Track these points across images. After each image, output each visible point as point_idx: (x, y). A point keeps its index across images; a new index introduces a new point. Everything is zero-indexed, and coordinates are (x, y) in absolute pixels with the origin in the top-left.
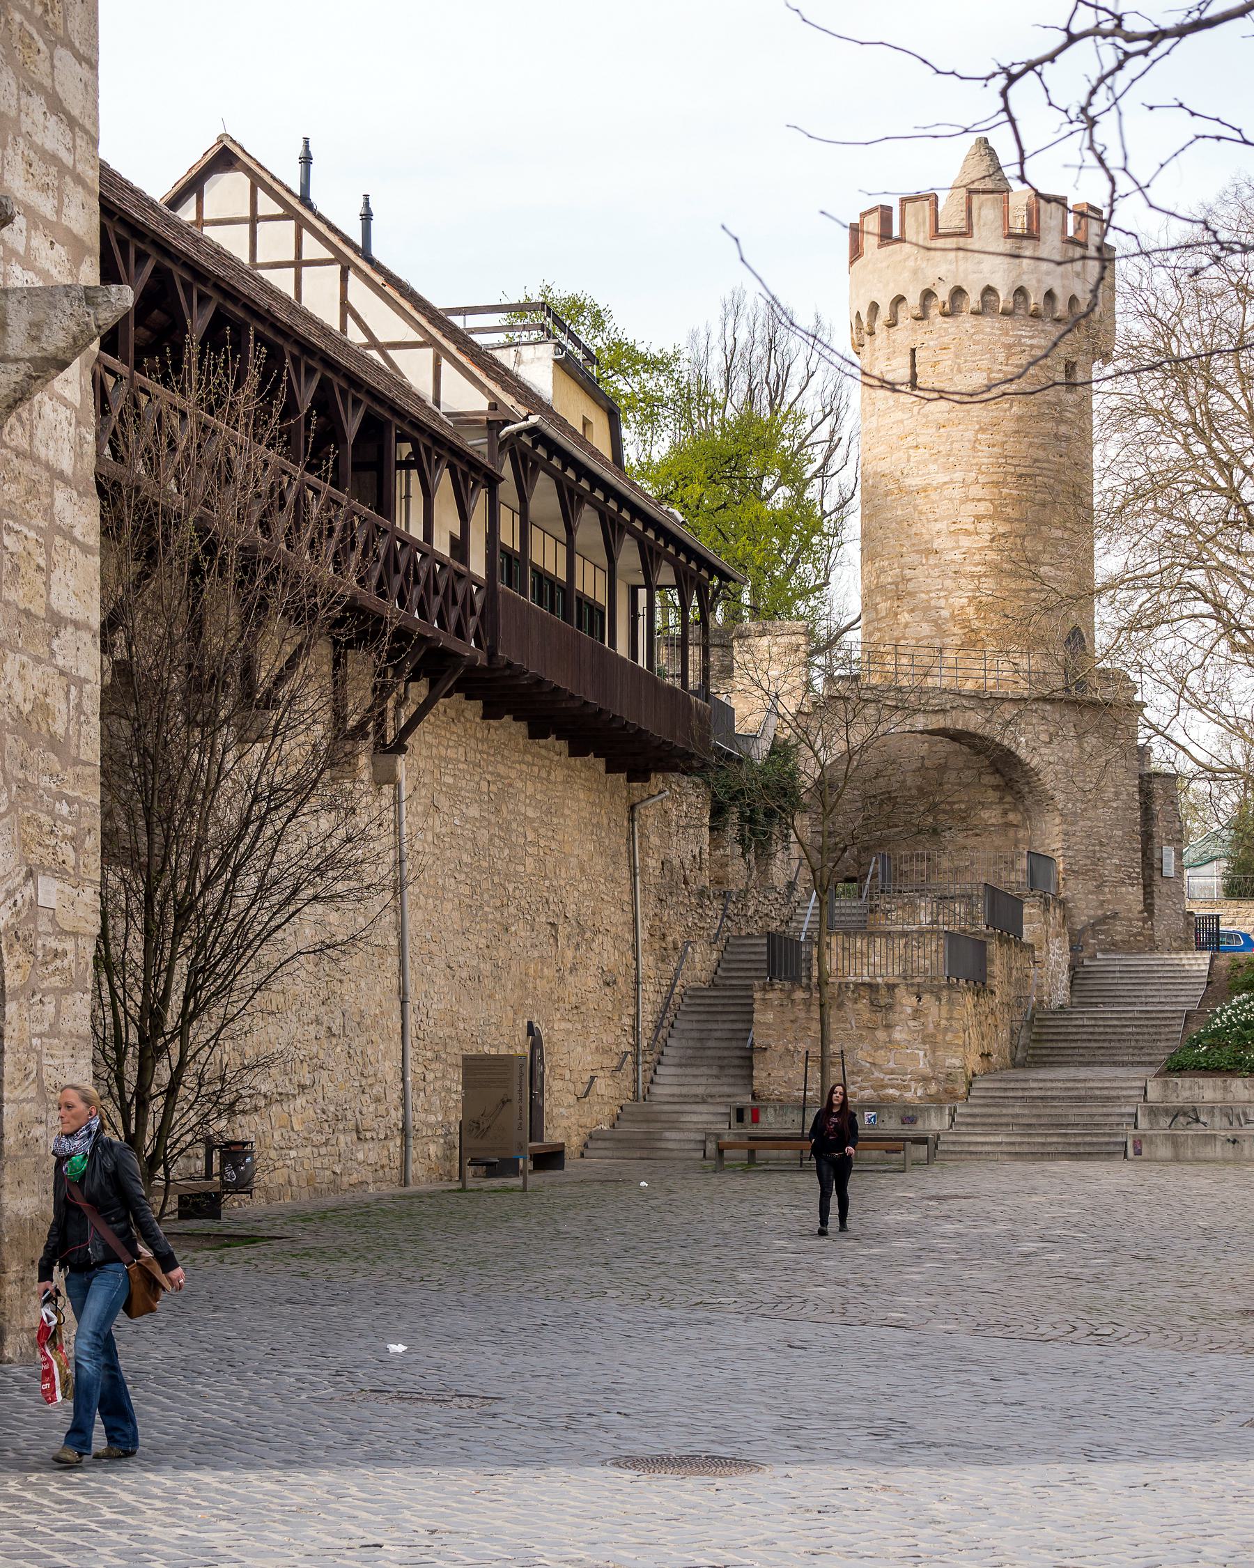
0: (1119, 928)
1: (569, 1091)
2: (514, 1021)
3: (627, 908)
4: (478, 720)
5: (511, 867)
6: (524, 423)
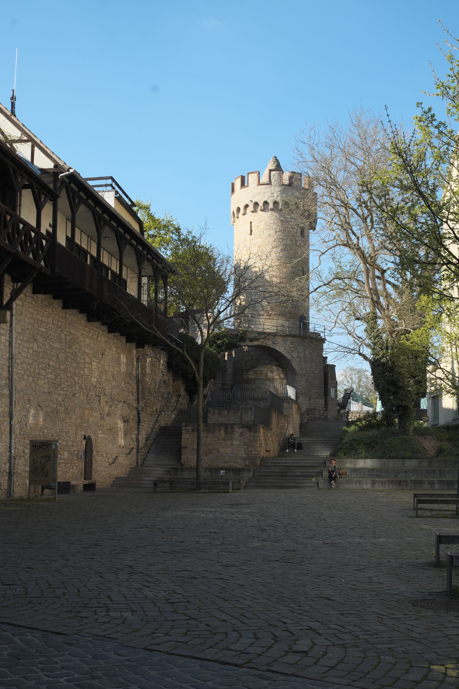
0: (316, 413)
1: (105, 461)
2: (76, 431)
3: (135, 394)
4: (60, 309)
5: (77, 371)
6: (68, 173)
